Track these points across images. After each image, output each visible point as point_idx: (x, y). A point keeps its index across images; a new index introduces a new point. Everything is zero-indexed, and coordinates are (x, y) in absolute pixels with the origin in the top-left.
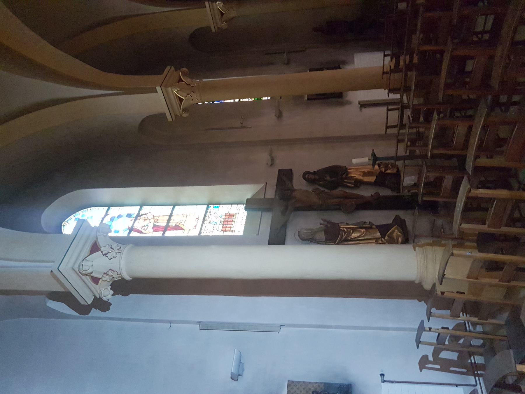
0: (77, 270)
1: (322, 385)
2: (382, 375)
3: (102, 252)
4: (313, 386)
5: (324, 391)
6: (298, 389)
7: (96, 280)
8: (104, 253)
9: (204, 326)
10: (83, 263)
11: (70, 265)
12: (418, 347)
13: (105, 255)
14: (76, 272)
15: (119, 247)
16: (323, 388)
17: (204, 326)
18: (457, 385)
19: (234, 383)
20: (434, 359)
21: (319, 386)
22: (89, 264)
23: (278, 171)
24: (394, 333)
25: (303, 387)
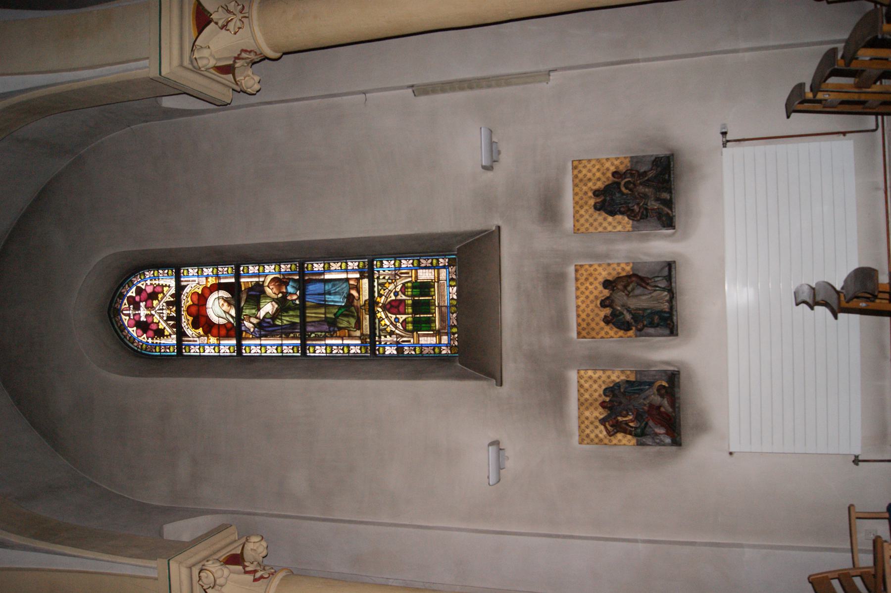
0: (190, 67)
1: (628, 160)
2: (724, 134)
3: (216, 23)
4: (612, 164)
5: (631, 170)
6: (590, 171)
7: (227, 70)
8: (220, 24)
9: (420, 90)
10: (196, 55)
11: (176, 62)
12: (788, 117)
13: (224, 27)
14: (188, 69)
15: (240, 7)
16: (629, 165)
17: (420, 90)
18: (844, 133)
19: (490, 174)
20: (831, 584)
21: (622, 163)
22: (205, 53)
23: (600, 216)
24: (747, 55)
25: (597, 167)
